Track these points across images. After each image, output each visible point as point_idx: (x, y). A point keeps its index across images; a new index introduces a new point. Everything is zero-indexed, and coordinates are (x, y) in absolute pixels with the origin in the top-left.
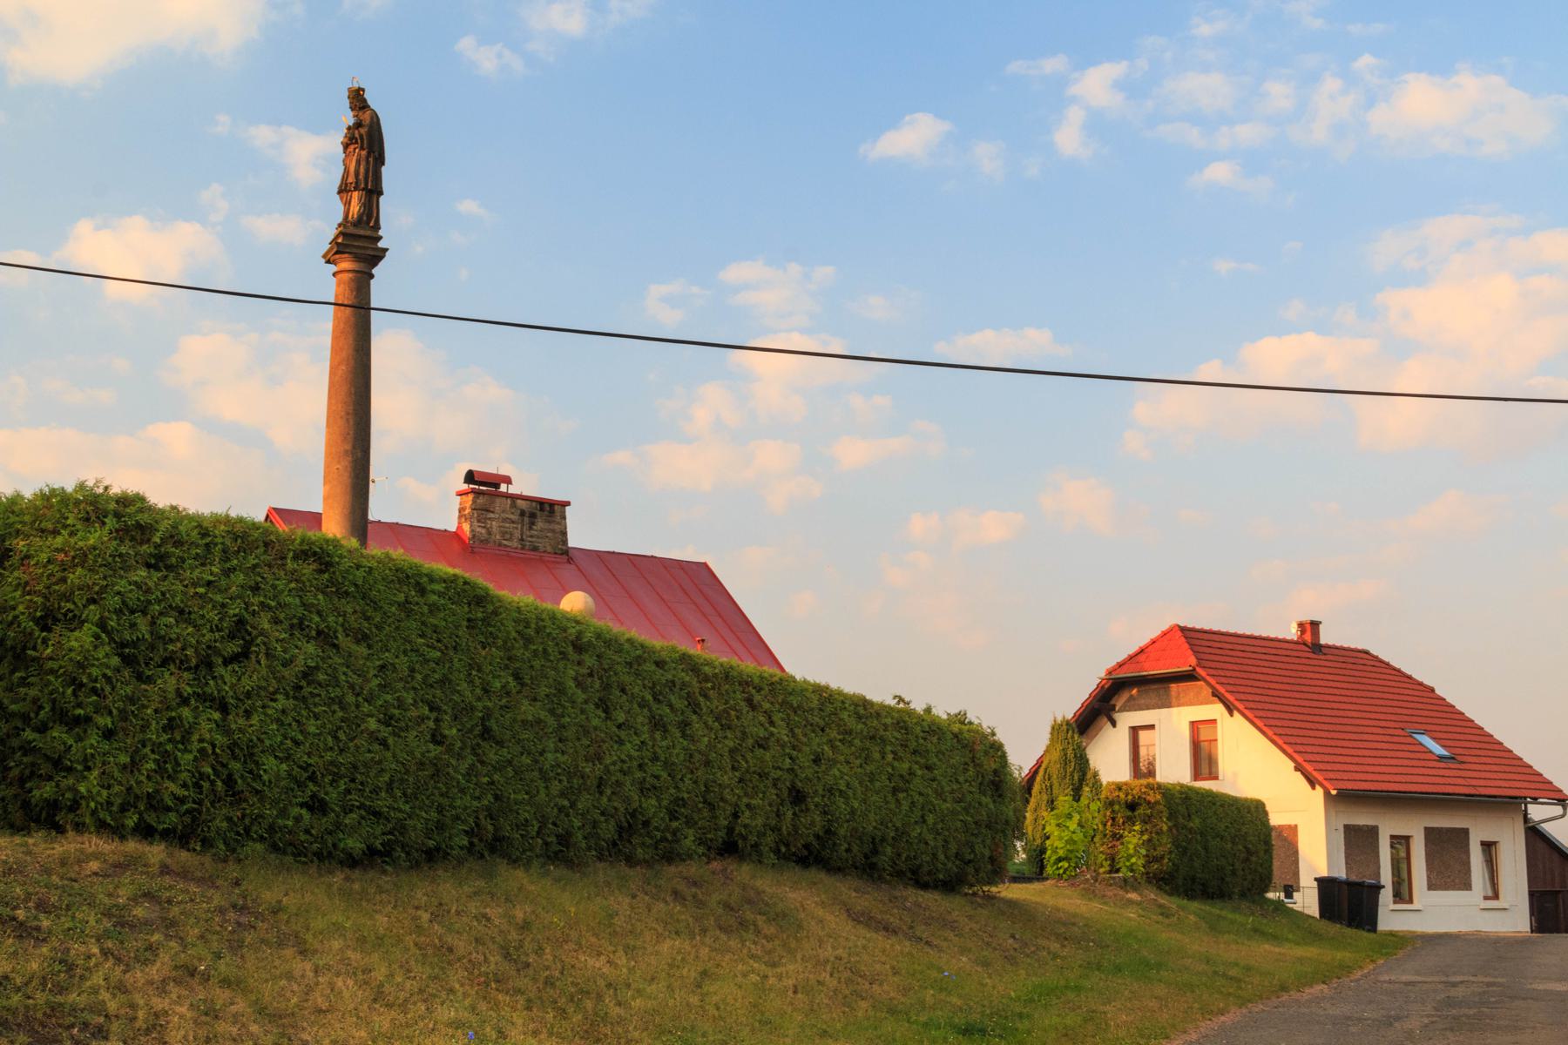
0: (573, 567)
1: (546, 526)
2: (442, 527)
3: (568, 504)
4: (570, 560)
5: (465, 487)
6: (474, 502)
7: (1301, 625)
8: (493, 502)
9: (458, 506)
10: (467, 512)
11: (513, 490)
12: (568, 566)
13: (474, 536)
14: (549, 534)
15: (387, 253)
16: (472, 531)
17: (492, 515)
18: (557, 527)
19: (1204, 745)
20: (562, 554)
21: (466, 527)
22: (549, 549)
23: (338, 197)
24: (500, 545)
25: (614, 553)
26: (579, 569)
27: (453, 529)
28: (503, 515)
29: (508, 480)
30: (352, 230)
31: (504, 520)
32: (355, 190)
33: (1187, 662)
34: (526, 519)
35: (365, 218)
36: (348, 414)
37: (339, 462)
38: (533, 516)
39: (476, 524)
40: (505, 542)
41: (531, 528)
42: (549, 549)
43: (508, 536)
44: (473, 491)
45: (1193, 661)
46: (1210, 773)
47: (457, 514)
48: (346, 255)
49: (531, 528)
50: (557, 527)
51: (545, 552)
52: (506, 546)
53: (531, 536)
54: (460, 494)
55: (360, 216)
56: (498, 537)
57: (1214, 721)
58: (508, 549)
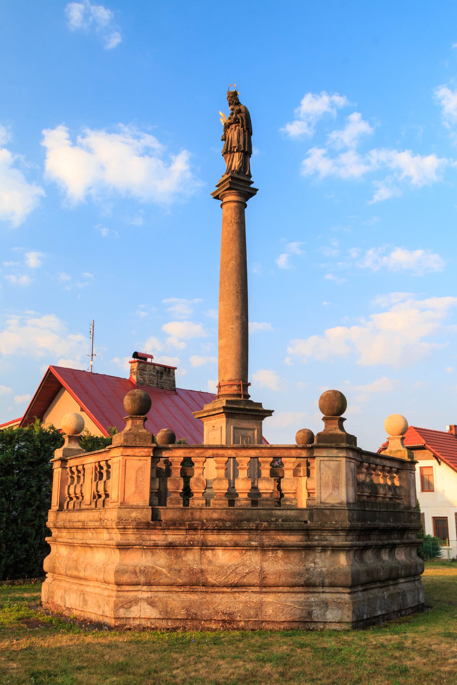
0: (178, 396)
1: (167, 378)
2: (124, 378)
3: (176, 368)
4: (176, 394)
5: (133, 359)
6: (138, 366)
7: (451, 427)
8: (146, 367)
9: (130, 368)
10: (134, 371)
11: (154, 361)
12: (175, 396)
13: (138, 382)
14: (168, 382)
15: (257, 192)
16: (137, 379)
17: (145, 372)
18: (171, 378)
19: (426, 477)
20: (173, 391)
21: (134, 377)
22: (168, 388)
23: (223, 158)
24: (148, 386)
25: (192, 391)
26: (181, 398)
27: (128, 378)
28: (149, 372)
29: (151, 357)
30: (236, 175)
31: (150, 375)
32: (237, 152)
33: (422, 442)
34: (159, 375)
35: (242, 170)
36: (237, 292)
37: (233, 324)
38: (162, 373)
39: (139, 376)
40: (151, 385)
41: (161, 379)
42: (168, 388)
43: (152, 382)
44: (138, 361)
45: (424, 442)
46: (429, 489)
47: (130, 371)
48: (234, 191)
49: (161, 379)
50: (171, 378)
51: (166, 389)
52: (151, 386)
53: (161, 382)
54: (131, 362)
55: (240, 169)
56: (148, 382)
57: (432, 467)
58: (151, 388)
